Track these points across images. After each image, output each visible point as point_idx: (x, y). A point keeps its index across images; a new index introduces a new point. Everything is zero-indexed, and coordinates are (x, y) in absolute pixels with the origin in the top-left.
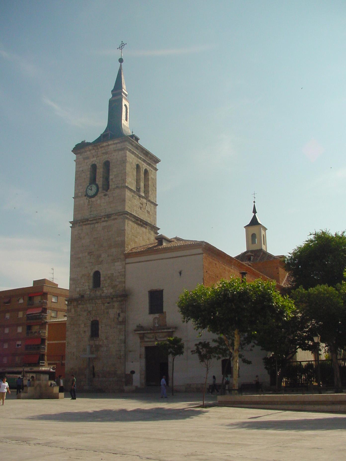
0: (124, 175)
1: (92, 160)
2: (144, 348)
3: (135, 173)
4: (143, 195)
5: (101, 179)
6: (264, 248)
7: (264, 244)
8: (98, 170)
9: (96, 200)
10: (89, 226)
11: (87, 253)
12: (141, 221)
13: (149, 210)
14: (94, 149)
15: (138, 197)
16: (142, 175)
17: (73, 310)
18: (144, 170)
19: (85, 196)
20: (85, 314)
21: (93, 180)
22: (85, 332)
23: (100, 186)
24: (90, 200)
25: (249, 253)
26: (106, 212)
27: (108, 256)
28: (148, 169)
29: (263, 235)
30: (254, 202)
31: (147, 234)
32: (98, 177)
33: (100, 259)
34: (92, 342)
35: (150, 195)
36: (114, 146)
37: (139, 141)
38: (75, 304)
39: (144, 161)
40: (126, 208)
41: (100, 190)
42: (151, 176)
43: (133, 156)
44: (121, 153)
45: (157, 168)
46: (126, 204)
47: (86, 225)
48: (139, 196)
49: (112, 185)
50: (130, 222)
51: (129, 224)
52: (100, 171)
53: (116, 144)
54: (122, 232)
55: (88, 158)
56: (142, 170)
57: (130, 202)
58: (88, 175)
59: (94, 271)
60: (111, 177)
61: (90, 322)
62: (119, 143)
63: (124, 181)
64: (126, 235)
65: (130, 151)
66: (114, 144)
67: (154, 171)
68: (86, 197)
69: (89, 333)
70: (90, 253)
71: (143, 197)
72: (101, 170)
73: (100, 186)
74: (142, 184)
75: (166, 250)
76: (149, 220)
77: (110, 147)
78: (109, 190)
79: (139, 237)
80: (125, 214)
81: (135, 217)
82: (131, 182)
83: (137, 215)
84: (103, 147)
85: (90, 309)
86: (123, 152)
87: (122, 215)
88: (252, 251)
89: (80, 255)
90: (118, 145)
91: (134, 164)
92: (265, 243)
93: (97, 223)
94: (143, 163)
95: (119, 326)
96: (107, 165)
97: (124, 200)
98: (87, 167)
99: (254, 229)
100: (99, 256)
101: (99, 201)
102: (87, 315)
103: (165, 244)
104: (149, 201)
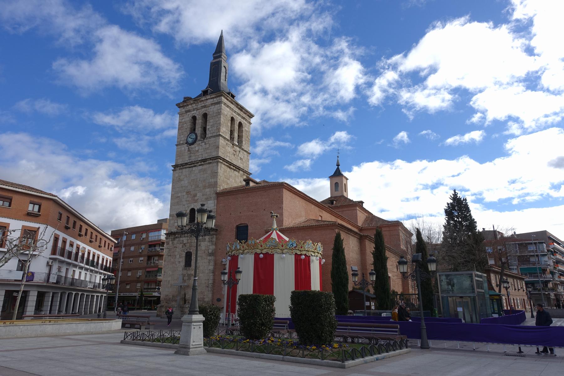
0: (218, 126)
1: (192, 112)
2: (37, 292)
3: (229, 124)
4: (237, 144)
5: (200, 129)
6: (345, 194)
7: (345, 191)
8: (197, 121)
9: (195, 147)
10: (188, 169)
11: (185, 193)
12: (234, 165)
13: (242, 157)
14: (194, 103)
15: (231, 145)
16: (236, 127)
17: (171, 243)
18: (238, 123)
19: (186, 143)
20: (181, 246)
21: (193, 130)
22: (179, 262)
23: (199, 135)
24: (190, 147)
25: (333, 199)
26: (202, 157)
27: (203, 195)
28: (242, 123)
29: (345, 184)
30: (338, 157)
31: (239, 177)
32: (197, 127)
33: (196, 198)
34: (185, 272)
35: (243, 144)
36: (212, 100)
37: (235, 98)
38: (173, 237)
39: (239, 115)
40: (219, 154)
41: (199, 138)
42: (245, 129)
43: (228, 109)
44: (216, 106)
45: (251, 122)
46: (220, 150)
47: (185, 168)
48: (233, 145)
49: (209, 134)
50: (223, 166)
51: (221, 168)
52: (199, 122)
53: (213, 98)
54: (215, 174)
55: (189, 111)
56: (237, 123)
57: (224, 149)
58: (188, 125)
59: (190, 208)
60: (208, 127)
61: (185, 253)
62: (215, 97)
63: (219, 130)
64: (219, 177)
65: (225, 104)
66: (211, 98)
67: (248, 124)
68: (186, 145)
69: (183, 264)
70: (188, 193)
71: (236, 146)
72: (200, 121)
73: (199, 135)
74: (236, 135)
75: (253, 189)
76: (241, 166)
77: (208, 101)
78: (206, 138)
79: (231, 179)
80: (217, 158)
81: (227, 162)
82: (225, 131)
83: (229, 161)
84: (202, 101)
85: (185, 241)
86: (218, 105)
87: (216, 159)
88: (335, 197)
89: (180, 195)
90: (215, 99)
91: (228, 116)
92: (346, 190)
93: (195, 166)
94: (237, 116)
95: (208, 257)
96: (205, 116)
97: (218, 147)
98: (188, 118)
99: (336, 180)
100: (195, 195)
101: (197, 147)
102: (183, 247)
103: (252, 184)
104: (243, 149)
